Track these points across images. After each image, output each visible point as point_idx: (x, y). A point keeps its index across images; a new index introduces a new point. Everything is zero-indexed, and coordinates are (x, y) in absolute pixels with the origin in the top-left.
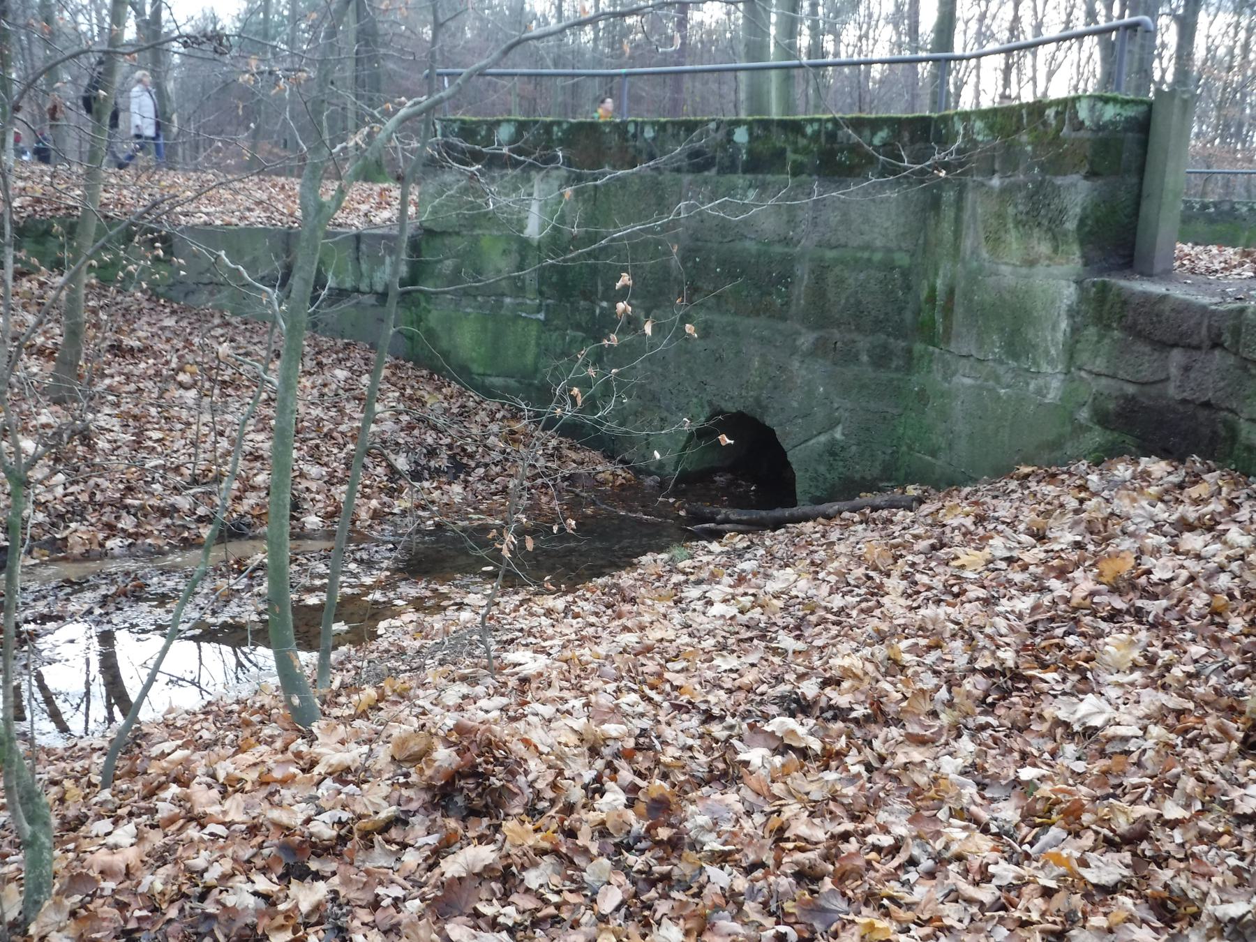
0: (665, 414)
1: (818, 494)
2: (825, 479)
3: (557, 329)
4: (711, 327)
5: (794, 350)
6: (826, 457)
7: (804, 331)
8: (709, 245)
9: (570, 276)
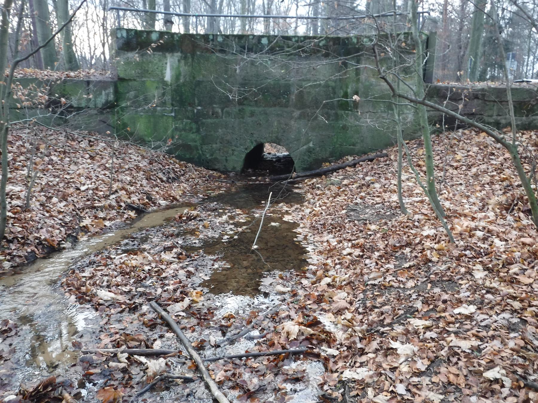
0: (234, 148)
1: (305, 166)
2: (308, 161)
3: (180, 119)
4: (254, 112)
5: (292, 118)
6: (307, 153)
7: (295, 110)
8: (252, 82)
9: (184, 97)
